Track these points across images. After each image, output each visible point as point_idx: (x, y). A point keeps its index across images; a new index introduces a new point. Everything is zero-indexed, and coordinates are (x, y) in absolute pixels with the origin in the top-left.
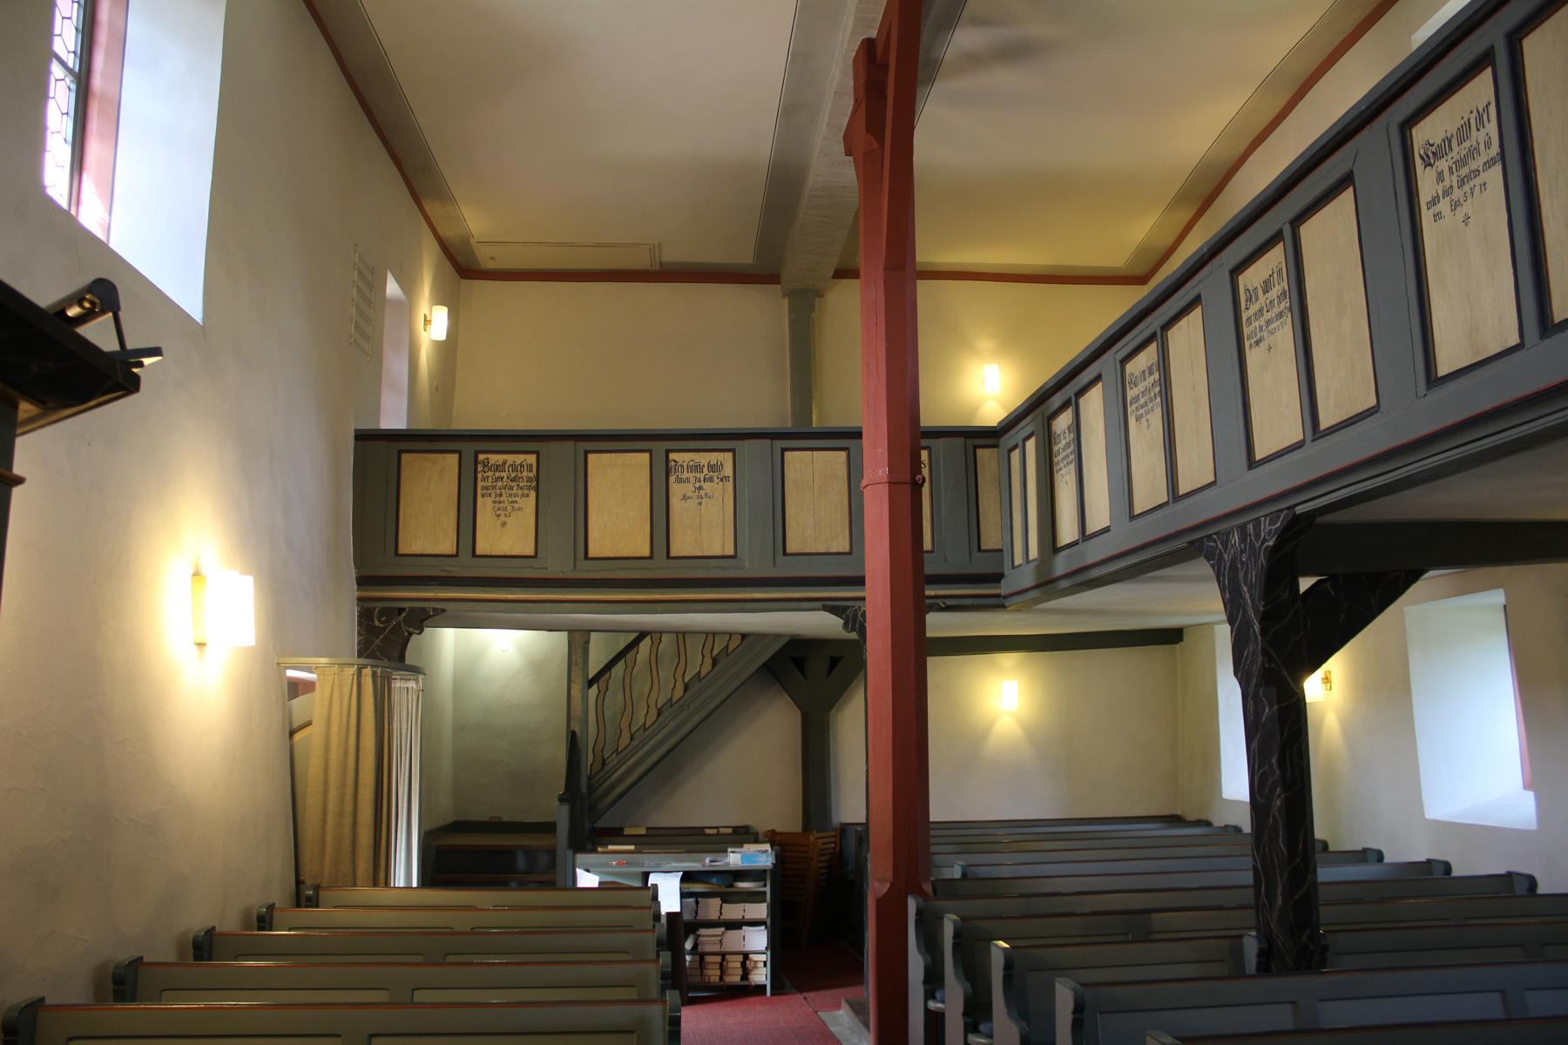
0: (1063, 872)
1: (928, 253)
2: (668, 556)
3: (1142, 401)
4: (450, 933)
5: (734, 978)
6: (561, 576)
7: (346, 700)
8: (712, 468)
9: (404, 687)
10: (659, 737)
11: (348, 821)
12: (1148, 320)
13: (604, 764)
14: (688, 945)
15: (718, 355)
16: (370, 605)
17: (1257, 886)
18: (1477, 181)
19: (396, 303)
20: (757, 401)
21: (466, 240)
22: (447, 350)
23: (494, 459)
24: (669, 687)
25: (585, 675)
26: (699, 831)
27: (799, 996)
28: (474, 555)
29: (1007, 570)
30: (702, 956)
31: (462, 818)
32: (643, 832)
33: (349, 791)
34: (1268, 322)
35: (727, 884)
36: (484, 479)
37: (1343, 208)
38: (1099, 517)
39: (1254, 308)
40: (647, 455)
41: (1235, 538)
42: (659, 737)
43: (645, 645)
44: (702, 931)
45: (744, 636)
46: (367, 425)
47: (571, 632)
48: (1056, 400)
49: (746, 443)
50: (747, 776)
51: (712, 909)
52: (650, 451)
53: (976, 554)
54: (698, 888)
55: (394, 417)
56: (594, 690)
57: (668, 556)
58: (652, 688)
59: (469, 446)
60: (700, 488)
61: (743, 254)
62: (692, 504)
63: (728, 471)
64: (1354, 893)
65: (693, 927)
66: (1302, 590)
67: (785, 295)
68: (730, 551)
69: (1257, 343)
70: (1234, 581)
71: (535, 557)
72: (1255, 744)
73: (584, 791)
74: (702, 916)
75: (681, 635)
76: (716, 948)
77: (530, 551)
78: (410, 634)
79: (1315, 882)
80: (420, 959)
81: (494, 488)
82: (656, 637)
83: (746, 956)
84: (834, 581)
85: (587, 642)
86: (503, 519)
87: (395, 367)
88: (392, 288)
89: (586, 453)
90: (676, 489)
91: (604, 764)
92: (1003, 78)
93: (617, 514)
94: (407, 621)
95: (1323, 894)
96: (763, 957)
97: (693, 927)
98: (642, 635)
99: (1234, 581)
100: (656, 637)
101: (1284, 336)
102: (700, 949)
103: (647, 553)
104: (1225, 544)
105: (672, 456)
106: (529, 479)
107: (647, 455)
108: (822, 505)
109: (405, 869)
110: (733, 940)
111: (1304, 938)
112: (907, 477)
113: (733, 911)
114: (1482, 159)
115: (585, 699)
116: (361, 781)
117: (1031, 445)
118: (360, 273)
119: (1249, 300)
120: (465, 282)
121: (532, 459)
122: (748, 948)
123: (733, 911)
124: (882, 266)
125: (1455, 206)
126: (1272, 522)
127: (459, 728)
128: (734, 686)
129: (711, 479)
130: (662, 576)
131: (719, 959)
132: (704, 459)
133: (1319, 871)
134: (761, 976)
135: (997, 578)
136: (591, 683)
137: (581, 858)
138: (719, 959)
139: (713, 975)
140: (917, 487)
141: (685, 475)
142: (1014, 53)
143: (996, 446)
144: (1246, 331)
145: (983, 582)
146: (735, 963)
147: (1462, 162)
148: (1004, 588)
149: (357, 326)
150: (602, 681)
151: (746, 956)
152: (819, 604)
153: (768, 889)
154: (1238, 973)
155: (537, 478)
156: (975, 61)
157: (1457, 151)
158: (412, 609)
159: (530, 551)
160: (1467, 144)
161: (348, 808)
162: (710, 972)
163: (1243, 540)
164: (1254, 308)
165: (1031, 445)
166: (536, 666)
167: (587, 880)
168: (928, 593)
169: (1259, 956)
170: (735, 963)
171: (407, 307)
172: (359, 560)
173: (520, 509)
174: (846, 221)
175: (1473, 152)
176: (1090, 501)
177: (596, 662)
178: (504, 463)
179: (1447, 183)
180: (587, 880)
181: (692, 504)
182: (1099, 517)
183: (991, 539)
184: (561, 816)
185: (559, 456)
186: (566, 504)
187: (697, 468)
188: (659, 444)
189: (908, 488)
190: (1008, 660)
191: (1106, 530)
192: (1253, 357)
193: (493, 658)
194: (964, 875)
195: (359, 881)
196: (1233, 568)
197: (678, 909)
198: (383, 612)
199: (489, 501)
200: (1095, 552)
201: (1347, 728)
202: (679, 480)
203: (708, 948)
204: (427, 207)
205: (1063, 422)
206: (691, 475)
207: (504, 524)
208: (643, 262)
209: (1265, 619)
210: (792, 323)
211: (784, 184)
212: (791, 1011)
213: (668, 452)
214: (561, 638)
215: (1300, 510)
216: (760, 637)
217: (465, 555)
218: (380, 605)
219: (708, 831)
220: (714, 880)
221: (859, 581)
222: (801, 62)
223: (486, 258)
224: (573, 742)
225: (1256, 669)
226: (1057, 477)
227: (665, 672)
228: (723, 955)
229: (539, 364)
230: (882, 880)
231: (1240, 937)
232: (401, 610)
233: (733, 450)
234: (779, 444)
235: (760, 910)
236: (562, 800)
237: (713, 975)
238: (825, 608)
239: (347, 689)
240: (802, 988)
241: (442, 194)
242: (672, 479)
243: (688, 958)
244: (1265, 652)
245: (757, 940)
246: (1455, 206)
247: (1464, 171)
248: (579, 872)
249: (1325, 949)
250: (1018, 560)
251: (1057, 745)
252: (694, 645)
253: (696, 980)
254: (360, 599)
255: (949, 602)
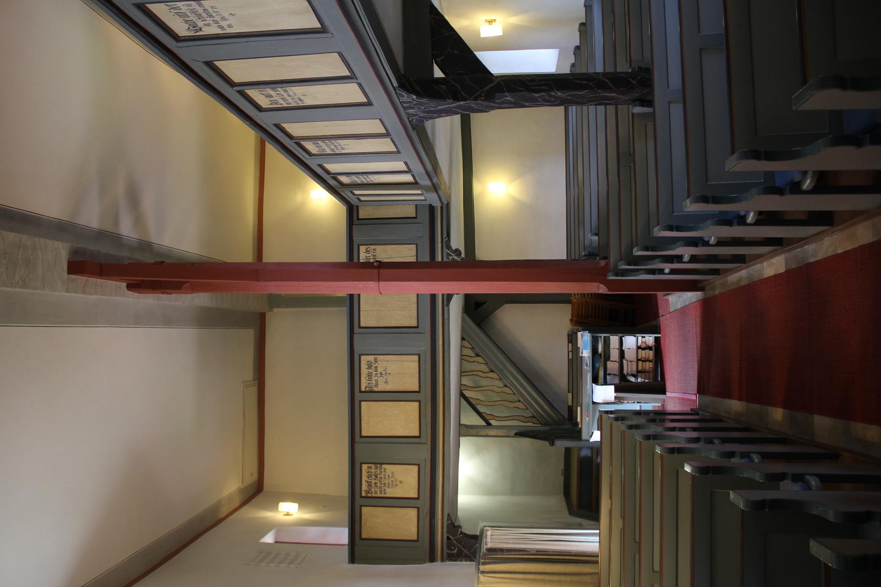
0: (594, 184)
1: (246, 256)
2: (419, 392)
3: (333, 147)
4: (623, 531)
5: (650, 354)
6: (429, 451)
7: (497, 580)
8: (370, 367)
9: (493, 539)
10: (518, 386)
11: (563, 578)
12: (291, 148)
13: (533, 417)
14: (633, 379)
15: (307, 346)
16: (445, 555)
17: (605, 105)
18: (210, 10)
19: (277, 535)
20: (332, 326)
21: (242, 491)
22: (303, 499)
23: (364, 487)
24: (493, 382)
25: (485, 428)
26: (571, 362)
27: (661, 318)
28: (418, 498)
29: (428, 203)
30: (638, 372)
31: (562, 491)
32: (570, 395)
33: (547, 577)
34: (289, 96)
35: (600, 357)
36: (376, 493)
37: (226, 66)
38: (400, 166)
39: (281, 101)
40: (363, 403)
41: (411, 111)
42: (518, 386)
43: (467, 393)
44: (625, 372)
45: (463, 339)
46: (345, 552)
47: (460, 435)
48: (332, 182)
49: (354, 238)
50: (541, 333)
51: (613, 366)
52: (360, 401)
53: (418, 220)
54: (601, 374)
55: (342, 535)
56: (493, 422)
57: (419, 392)
58: (491, 388)
59: (356, 503)
60: (381, 374)
61: (248, 335)
62: (390, 378)
63: (371, 358)
64: (611, 48)
65: (623, 377)
66: (442, 75)
67: (272, 310)
68: (416, 358)
69: (301, 100)
70: (434, 112)
71: (419, 401)
72: (527, 104)
73: (547, 428)
74: (617, 372)
75: (462, 373)
76: (634, 364)
77: (416, 468)
78: (461, 533)
79: (605, 74)
80: (637, 556)
81: (381, 488)
82: (463, 388)
83: (639, 348)
84: (433, 307)
85: (466, 426)
86: (398, 483)
87: (313, 534)
88: (269, 539)
89: (362, 437)
90: (382, 387)
91: (533, 417)
92: (148, 204)
93: (396, 420)
94: (455, 535)
95: (610, 69)
96: (640, 338)
97: (623, 377)
98: (462, 395)
99: (434, 112)
100: (463, 388)
101: (298, 90)
102: (635, 373)
103: (417, 404)
104: (414, 115)
105: (363, 389)
106: (376, 468)
107: (363, 403)
108: (391, 305)
109: (587, 541)
110: (630, 355)
111: (634, 82)
112: (375, 271)
113: (614, 354)
114: (198, 8)
115: (497, 427)
116: (541, 571)
117: (356, 192)
118: (261, 561)
119: (277, 104)
120: (265, 489)
121: (365, 467)
122: (634, 347)
123: (614, 354)
124: (256, 282)
125: (224, 19)
126: (403, 96)
127: (513, 492)
128: (491, 345)
129: (376, 368)
130: (430, 395)
131: (640, 362)
132: (364, 371)
133: (597, 71)
134: (650, 339)
135: (432, 208)
136: (489, 424)
137: (584, 436)
138: (640, 362)
139: (649, 366)
140: (381, 265)
141: (374, 382)
142: (134, 199)
143: (358, 207)
144: (294, 105)
145: (434, 217)
146: (643, 354)
147: (200, 16)
148: (437, 204)
149: (291, 563)
150: (487, 417)
151: (639, 348)
152: (446, 308)
153: (603, 335)
154: (653, 116)
155: (376, 464)
156: (139, 221)
157: (193, 18)
158: (448, 532)
159: (416, 468)
160: (189, 14)
161: (557, 578)
162: (647, 367)
163: (413, 108)
164: (281, 101)
165: (356, 192)
166: (479, 451)
167: (596, 436)
168: (440, 260)
169: (643, 106)
170: (643, 354)
171: (280, 527)
172: (422, 562)
173: (392, 473)
174: (232, 291)
175: (194, 12)
176: (392, 168)
177: (477, 421)
178: (367, 482)
179: (211, 22)
180: (596, 436)
181: (390, 378)
182: (400, 166)
183: (410, 211)
184: (562, 444)
185: (362, 450)
186: (390, 447)
187: (370, 375)
188: (356, 397)
189: (381, 270)
190: (477, 188)
191: (406, 163)
192: (308, 102)
193: (476, 475)
194: (596, 234)
195: (596, 571)
196: (427, 112)
197: (613, 387)
198: (449, 548)
199: (388, 490)
200: (417, 168)
201: (517, 13)
202: (377, 385)
203: (634, 368)
204: (222, 515)
205: (344, 179)
206: (374, 379)
207: (401, 482)
208: (254, 391)
209: (456, 98)
210: (287, 306)
211: (209, 319)
212: (667, 322)
213: (361, 392)
214: (463, 440)
215: (396, 84)
216: (463, 330)
217: (418, 503)
218: (445, 549)
219: (570, 357)
220: (597, 365)
221: (433, 297)
222: (139, 320)
223: (251, 478)
224: (521, 434)
225: (484, 103)
226: (375, 182)
227: (484, 382)
228: (638, 360)
229: (312, 450)
230: (599, 288)
231: (633, 114)
232: (448, 538)
233: (360, 355)
234: (356, 329)
235: (614, 340)
236: (552, 444)
237: (649, 366)
238: (448, 305)
239: (492, 580)
240: (656, 316)
241: (217, 507)
242: (376, 389)
243: (639, 380)
244: (475, 99)
245: (630, 341)
246: (224, 19)
247: (204, 15)
248: (592, 440)
249: (640, 69)
250: (423, 198)
251: (525, 161)
252: (468, 366)
253: (651, 375)
254: (442, 560)
255: (445, 235)
